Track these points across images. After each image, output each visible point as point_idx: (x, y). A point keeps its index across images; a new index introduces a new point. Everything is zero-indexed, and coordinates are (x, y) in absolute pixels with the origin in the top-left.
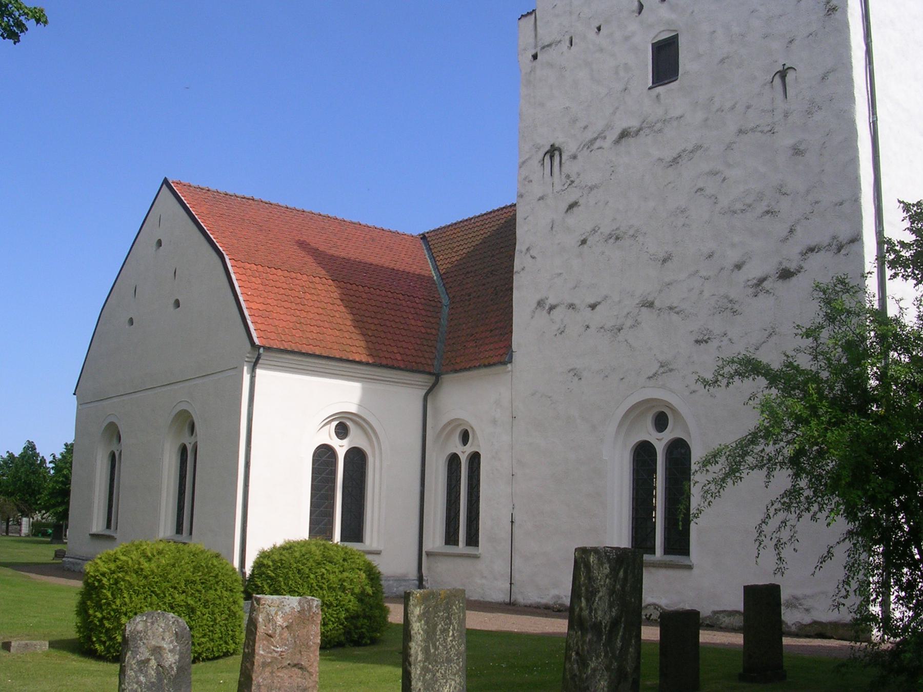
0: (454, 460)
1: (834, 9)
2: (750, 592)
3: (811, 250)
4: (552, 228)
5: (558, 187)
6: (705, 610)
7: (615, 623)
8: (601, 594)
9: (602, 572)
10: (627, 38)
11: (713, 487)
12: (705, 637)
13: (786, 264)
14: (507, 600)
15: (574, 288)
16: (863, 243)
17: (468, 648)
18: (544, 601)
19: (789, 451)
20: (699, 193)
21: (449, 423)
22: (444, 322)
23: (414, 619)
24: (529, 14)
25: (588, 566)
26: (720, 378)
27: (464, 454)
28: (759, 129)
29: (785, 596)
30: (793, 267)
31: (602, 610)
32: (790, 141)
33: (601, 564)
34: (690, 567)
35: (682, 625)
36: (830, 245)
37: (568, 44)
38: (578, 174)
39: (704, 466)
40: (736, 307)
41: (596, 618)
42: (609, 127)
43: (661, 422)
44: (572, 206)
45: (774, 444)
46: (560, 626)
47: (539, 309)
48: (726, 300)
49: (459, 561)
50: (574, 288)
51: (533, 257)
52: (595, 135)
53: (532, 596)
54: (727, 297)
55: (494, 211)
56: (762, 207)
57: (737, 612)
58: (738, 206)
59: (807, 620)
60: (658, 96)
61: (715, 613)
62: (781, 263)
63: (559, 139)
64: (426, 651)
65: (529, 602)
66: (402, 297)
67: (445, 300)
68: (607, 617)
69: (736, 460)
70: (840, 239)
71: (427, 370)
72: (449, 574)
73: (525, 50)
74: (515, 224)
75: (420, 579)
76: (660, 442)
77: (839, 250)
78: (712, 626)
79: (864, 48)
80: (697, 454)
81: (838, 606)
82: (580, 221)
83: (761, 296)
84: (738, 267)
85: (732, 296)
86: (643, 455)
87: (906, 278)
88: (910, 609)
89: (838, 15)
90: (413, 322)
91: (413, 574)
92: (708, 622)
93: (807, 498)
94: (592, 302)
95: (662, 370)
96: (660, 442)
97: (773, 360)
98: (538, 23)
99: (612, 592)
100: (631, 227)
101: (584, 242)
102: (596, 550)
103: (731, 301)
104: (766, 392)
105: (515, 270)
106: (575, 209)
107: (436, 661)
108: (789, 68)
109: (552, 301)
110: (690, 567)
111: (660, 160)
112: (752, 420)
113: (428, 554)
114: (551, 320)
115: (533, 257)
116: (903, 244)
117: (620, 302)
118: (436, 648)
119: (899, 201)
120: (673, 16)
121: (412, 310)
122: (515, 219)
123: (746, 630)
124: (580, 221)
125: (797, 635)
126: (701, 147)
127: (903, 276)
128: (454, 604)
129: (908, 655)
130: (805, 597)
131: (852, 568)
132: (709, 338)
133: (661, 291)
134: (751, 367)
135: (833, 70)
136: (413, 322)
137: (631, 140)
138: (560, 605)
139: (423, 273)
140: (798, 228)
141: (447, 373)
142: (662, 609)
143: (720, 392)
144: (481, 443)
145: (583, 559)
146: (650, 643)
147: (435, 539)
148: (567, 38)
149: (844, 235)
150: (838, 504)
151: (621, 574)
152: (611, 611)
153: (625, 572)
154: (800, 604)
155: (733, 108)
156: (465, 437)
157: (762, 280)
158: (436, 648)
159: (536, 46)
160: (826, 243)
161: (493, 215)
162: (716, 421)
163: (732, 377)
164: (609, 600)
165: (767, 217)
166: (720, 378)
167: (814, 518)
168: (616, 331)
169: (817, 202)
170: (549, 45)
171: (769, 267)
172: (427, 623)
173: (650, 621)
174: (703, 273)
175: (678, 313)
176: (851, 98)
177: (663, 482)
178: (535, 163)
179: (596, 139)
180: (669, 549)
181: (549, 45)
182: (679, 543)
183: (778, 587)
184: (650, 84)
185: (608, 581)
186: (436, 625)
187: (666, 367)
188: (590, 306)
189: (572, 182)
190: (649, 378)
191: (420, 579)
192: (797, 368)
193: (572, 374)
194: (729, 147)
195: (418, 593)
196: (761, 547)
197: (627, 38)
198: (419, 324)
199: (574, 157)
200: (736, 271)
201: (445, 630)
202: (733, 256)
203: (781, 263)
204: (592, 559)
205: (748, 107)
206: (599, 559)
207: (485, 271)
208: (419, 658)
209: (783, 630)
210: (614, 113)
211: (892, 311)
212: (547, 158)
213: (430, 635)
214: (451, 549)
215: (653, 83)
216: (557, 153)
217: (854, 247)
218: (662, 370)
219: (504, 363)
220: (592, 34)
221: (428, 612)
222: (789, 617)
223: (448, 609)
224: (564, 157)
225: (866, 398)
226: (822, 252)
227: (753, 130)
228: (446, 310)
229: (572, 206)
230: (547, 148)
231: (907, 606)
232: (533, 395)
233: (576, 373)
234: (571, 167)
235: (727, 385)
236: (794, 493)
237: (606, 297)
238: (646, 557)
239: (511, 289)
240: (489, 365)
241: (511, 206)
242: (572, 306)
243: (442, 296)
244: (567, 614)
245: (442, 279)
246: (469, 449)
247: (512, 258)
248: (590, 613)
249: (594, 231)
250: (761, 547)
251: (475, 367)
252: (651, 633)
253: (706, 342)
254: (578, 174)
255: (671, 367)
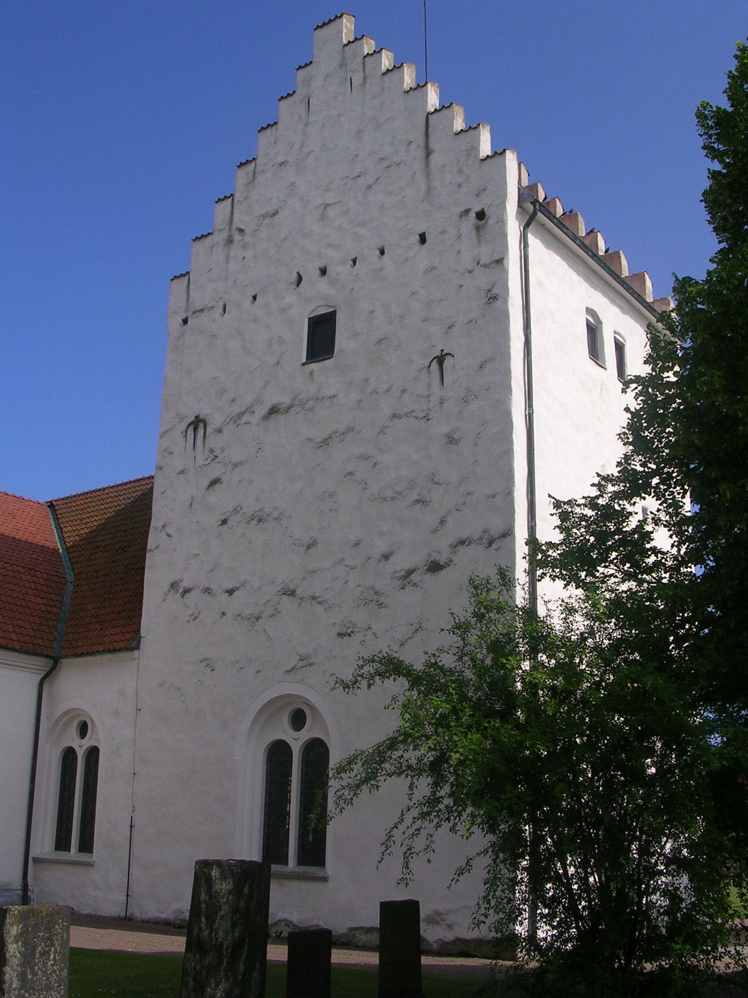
0: (69, 755)
1: (495, 298)
2: (388, 909)
3: (462, 543)
4: (191, 505)
5: (200, 462)
6: (339, 925)
7: (237, 946)
8: (223, 912)
9: (223, 887)
10: (283, 310)
11: (346, 792)
12: (338, 956)
13: (435, 557)
14: (123, 914)
15: (212, 571)
16: (514, 538)
17: (71, 971)
18: (164, 916)
19: (431, 757)
20: (348, 477)
21: (66, 713)
22: (67, 600)
23: (10, 940)
24: (182, 275)
25: (209, 881)
26: (359, 678)
27: (81, 748)
28: (414, 414)
29: (423, 913)
30: (442, 560)
31: (225, 932)
32: (445, 429)
33: (223, 877)
34: (325, 879)
35: (312, 944)
36: (480, 538)
37: (221, 310)
38: (223, 449)
39: (339, 773)
40: (382, 599)
41: (216, 939)
42: (258, 401)
43: (298, 720)
44: (214, 482)
45: (415, 749)
46: (177, 944)
47: (172, 592)
48: (372, 592)
49: (70, 869)
50: (212, 571)
51: (169, 536)
52: (243, 409)
53: (150, 910)
54: (373, 588)
55: (130, 482)
56: (413, 496)
57: (374, 929)
58: (389, 493)
59: (450, 936)
60: (311, 373)
61: (351, 929)
62: (430, 555)
63: (204, 411)
64: (22, 977)
65: (146, 917)
66: (21, 570)
67: (70, 576)
68: (229, 938)
69: (374, 764)
70: (492, 533)
71: (46, 653)
72: (60, 885)
73: (175, 313)
74: (152, 497)
75: (25, 888)
76: (297, 741)
77: (490, 544)
78: (348, 943)
79: (523, 339)
80: (336, 758)
81: (478, 925)
82: (221, 500)
83: (409, 588)
84: (386, 557)
85: (378, 588)
86: (278, 754)
87: (553, 578)
88: (553, 928)
89: (498, 304)
90: (32, 598)
91: (17, 884)
92: (344, 940)
93: (447, 807)
94: (230, 586)
95: (301, 664)
96: (297, 741)
97: (416, 660)
98: (191, 286)
99: (235, 910)
100: (275, 509)
101: (224, 522)
102: (219, 863)
103: (376, 593)
104: (408, 693)
105: (148, 548)
106: (217, 486)
107: (33, 989)
108: (447, 354)
109: (186, 584)
110: (325, 879)
111: (310, 440)
112: (393, 723)
113: (36, 860)
114: (185, 604)
115: (169, 536)
116: (550, 545)
117: (259, 588)
118: (34, 974)
119: (550, 496)
120: (332, 292)
121: (32, 585)
122: (152, 492)
123: (382, 949)
124: (221, 500)
125: (439, 954)
126: (353, 429)
127: (551, 576)
128: (57, 923)
129: (551, 976)
130: (448, 912)
131: (492, 882)
132: (352, 632)
133: (304, 579)
134: (393, 667)
135: (492, 359)
136: (32, 598)
137: (281, 417)
138: (181, 920)
139: (47, 544)
140: (450, 519)
141: (67, 657)
142: (293, 925)
143: (363, 692)
144: (99, 737)
145: (203, 871)
146: (277, 964)
147: (44, 842)
148: (221, 304)
149: (496, 528)
150: (473, 816)
151: (246, 890)
152: (233, 931)
153: (251, 887)
154: (443, 920)
155: (388, 391)
156: (83, 729)
157: (410, 572)
158: (34, 974)
159: (187, 310)
160: (477, 537)
161: (129, 486)
162: (356, 723)
163: (372, 677)
164: (232, 919)
165: (418, 506)
166: (359, 678)
167: (453, 829)
168: (254, 619)
169: (469, 494)
170: (202, 310)
171: (418, 559)
172: (25, 944)
173: (279, 940)
174: (349, 562)
175: (320, 603)
176: (508, 389)
177: (299, 786)
178: (177, 435)
179: (243, 413)
180: (302, 860)
181: (202, 310)
182: (313, 853)
183: (417, 902)
184: (304, 360)
185: (231, 900)
186: (34, 948)
187: (306, 661)
188: (227, 591)
189: (216, 457)
190: (288, 672)
191: (25, 888)
192: (441, 668)
193: (204, 664)
194: (382, 431)
195: (16, 909)
196: (400, 859)
197: (283, 310)
198: (39, 601)
199: (220, 431)
200: (383, 560)
201: (45, 952)
202: (382, 546)
203: (430, 555)
204: (215, 873)
205: (404, 391)
206: (221, 873)
207: (117, 546)
208: (14, 986)
209: (422, 948)
210: (264, 387)
211: (541, 611)
212: (191, 428)
213: (28, 958)
214: (63, 855)
215: (307, 359)
216: (201, 425)
217: (505, 541)
218: (301, 664)
219: (132, 649)
220: (247, 302)
221: (26, 932)
222: (430, 933)
223: (49, 929)
224: (209, 430)
225: (511, 700)
226: (473, 546)
227: (406, 415)
228: (70, 587)
229: (214, 482)
230: (192, 419)
231: (550, 925)
232: (161, 685)
233: (208, 664)
234: (214, 441)
235: (369, 687)
236: (433, 801)
237: (244, 583)
238: (274, 868)
239: (143, 568)
240: (115, 651)
241: (149, 478)
242: (207, 590)
243: (67, 571)
244: (185, 931)
245: (69, 553)
246: (87, 743)
247: (146, 534)
248: (210, 933)
249: (236, 510)
250: (400, 859)
251: (99, 652)
252: (277, 953)
253: (350, 636)
254: (223, 449)
255: (311, 661)
